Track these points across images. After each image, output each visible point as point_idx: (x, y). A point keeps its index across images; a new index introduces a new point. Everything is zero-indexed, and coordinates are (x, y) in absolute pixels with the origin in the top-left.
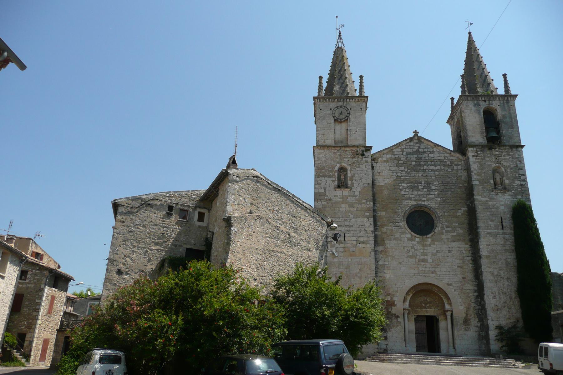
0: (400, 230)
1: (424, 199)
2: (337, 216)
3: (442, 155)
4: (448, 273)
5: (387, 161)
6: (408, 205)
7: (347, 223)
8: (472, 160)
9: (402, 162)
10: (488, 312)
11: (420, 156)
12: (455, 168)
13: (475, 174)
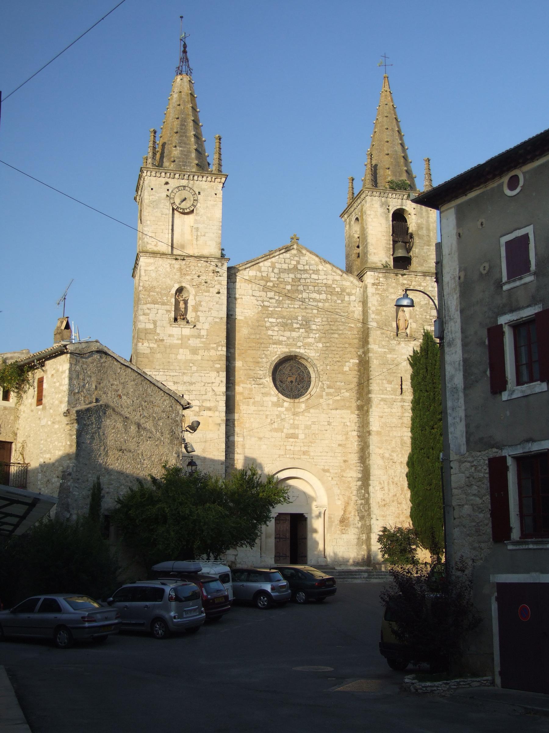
0: (263, 390)
1: (300, 344)
2: (172, 368)
3: (330, 277)
6: (278, 352)
7: (186, 379)
8: (371, 290)
9: (271, 284)
10: (372, 509)
11: (299, 276)
13: (373, 312)
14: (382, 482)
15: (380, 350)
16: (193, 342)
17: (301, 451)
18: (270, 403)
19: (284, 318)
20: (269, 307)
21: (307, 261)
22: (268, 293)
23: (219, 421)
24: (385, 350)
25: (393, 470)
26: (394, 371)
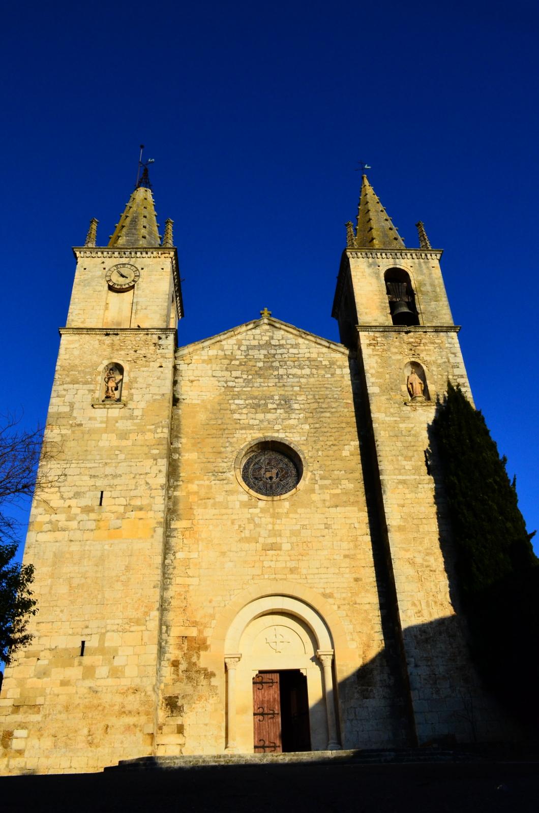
0: (228, 487)
2: (89, 457)
4: (324, 570)
5: (210, 361)
7: (109, 470)
11: (273, 352)
12: (338, 371)
14: (417, 603)
15: (387, 419)
16: (121, 425)
17: (286, 567)
18: (238, 504)
19: (256, 398)
20: (235, 387)
21: (282, 335)
22: (233, 372)
23: (153, 523)
24: (395, 419)
25: (432, 583)
26: (412, 444)
